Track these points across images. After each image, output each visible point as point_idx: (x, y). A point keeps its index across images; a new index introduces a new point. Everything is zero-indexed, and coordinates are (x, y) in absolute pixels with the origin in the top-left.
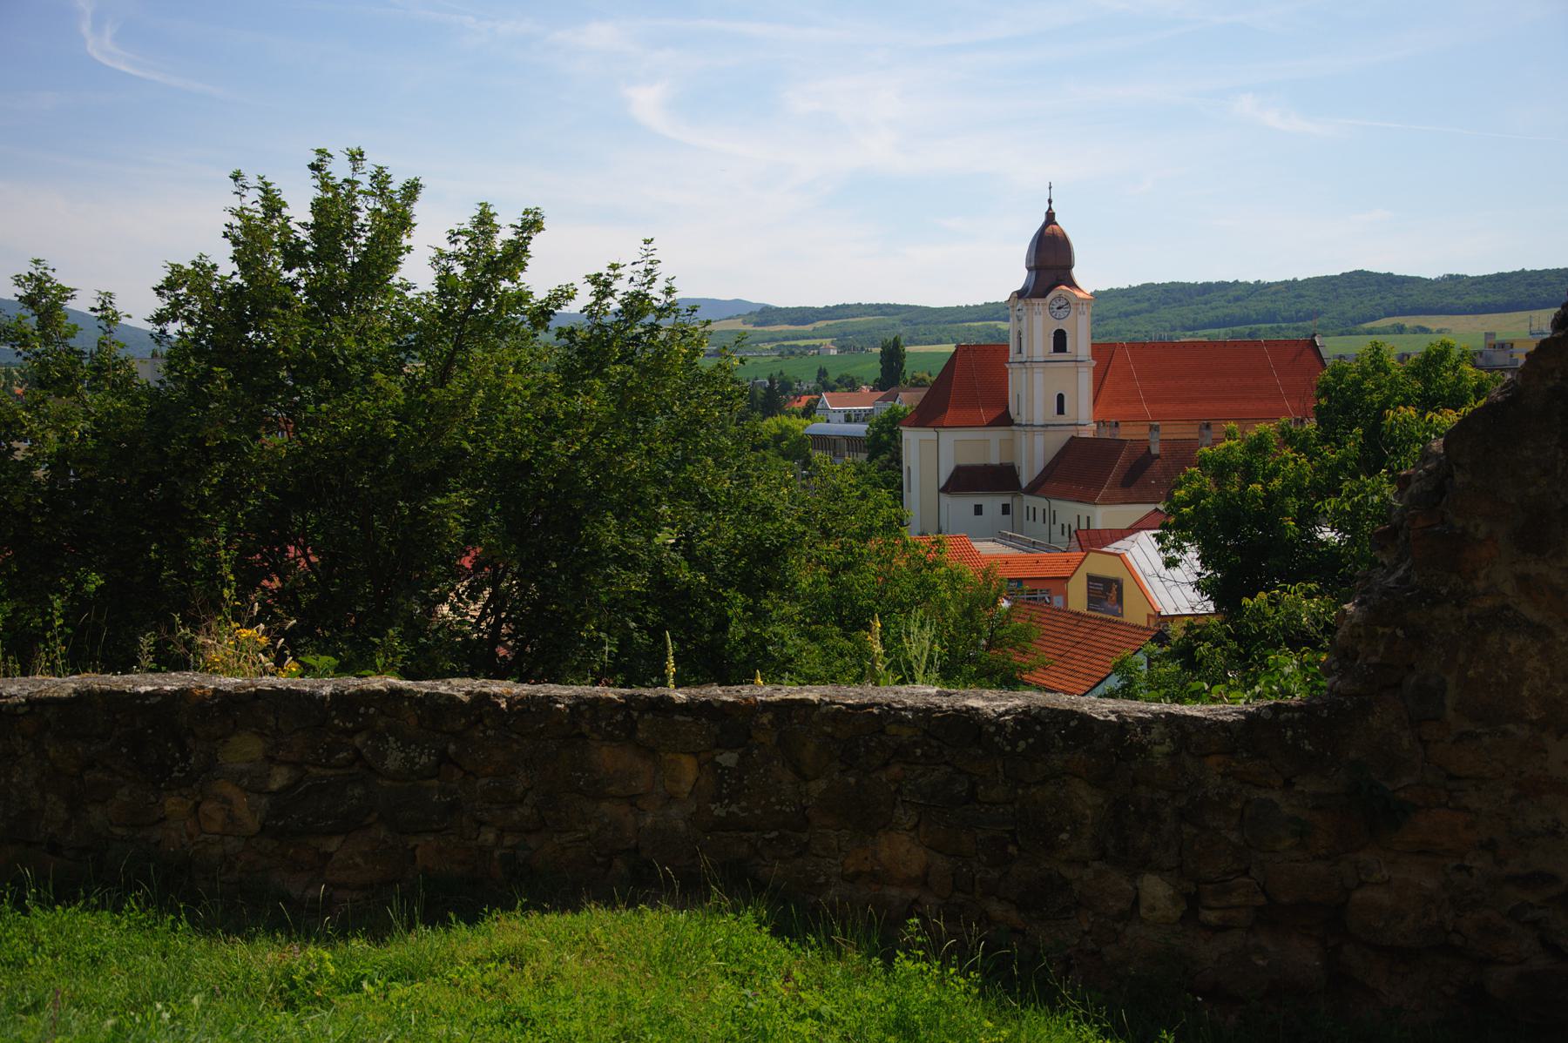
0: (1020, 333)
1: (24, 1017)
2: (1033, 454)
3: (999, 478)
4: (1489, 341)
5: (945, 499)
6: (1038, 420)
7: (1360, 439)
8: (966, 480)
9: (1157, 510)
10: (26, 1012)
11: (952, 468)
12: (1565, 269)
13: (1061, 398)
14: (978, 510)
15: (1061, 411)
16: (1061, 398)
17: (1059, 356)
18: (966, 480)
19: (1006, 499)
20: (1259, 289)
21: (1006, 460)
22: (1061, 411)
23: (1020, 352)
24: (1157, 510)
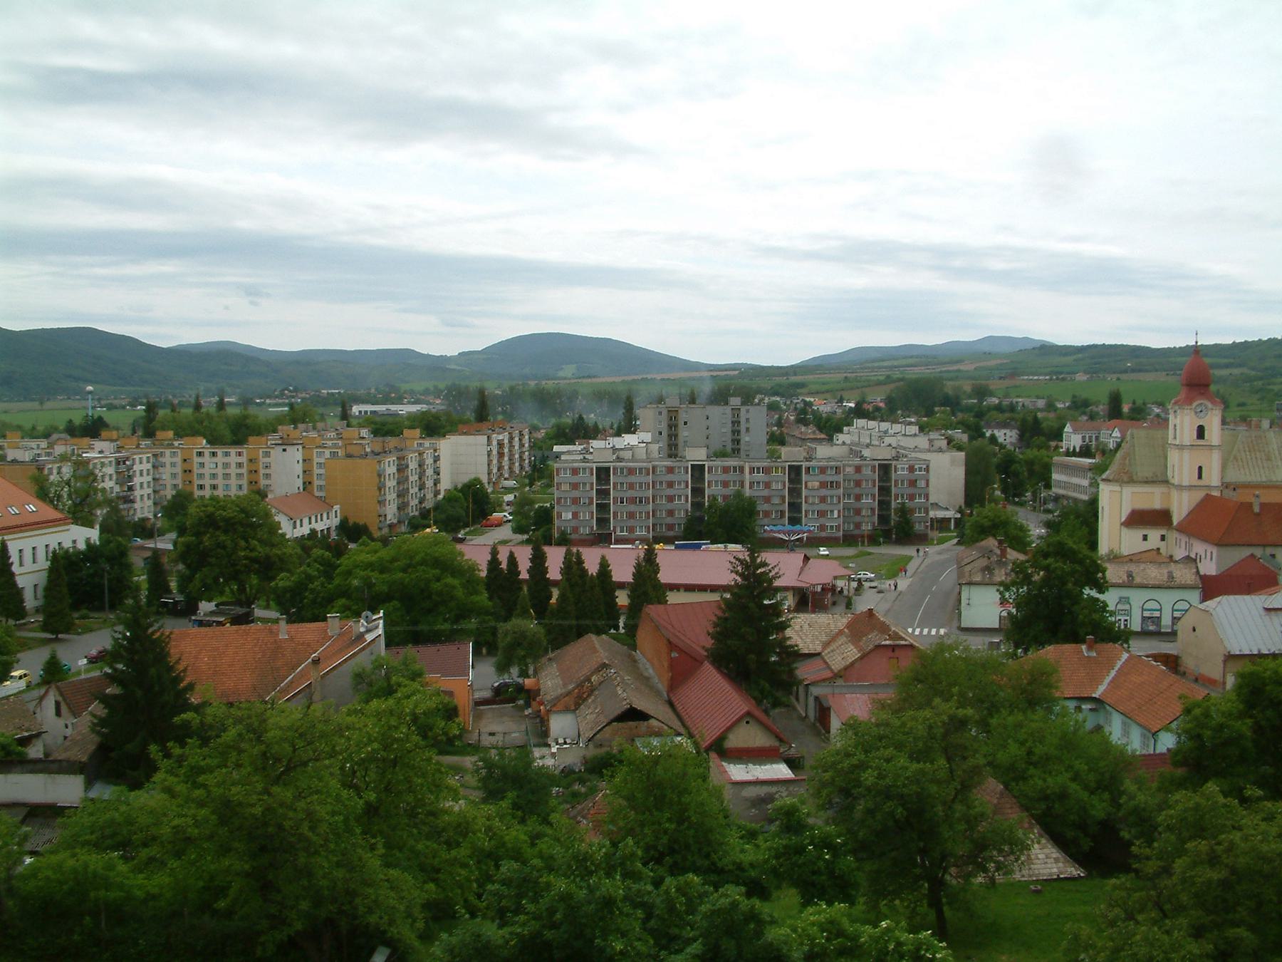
0: (1175, 426)
1: (961, 712)
2: (1180, 506)
3: (1159, 518)
4: (255, 488)
5: (1125, 531)
6: (1186, 483)
7: (340, 777)
8: (1139, 519)
9: (1252, 556)
10: (887, 737)
11: (1129, 511)
12: (1273, 343)
13: (1200, 468)
14: (1145, 538)
15: (1200, 477)
16: (1200, 468)
17: (1201, 442)
18: (1139, 519)
19: (1163, 532)
20: (781, 367)
21: (1165, 506)
22: (1200, 477)
23: (1175, 438)
24: (1252, 556)
